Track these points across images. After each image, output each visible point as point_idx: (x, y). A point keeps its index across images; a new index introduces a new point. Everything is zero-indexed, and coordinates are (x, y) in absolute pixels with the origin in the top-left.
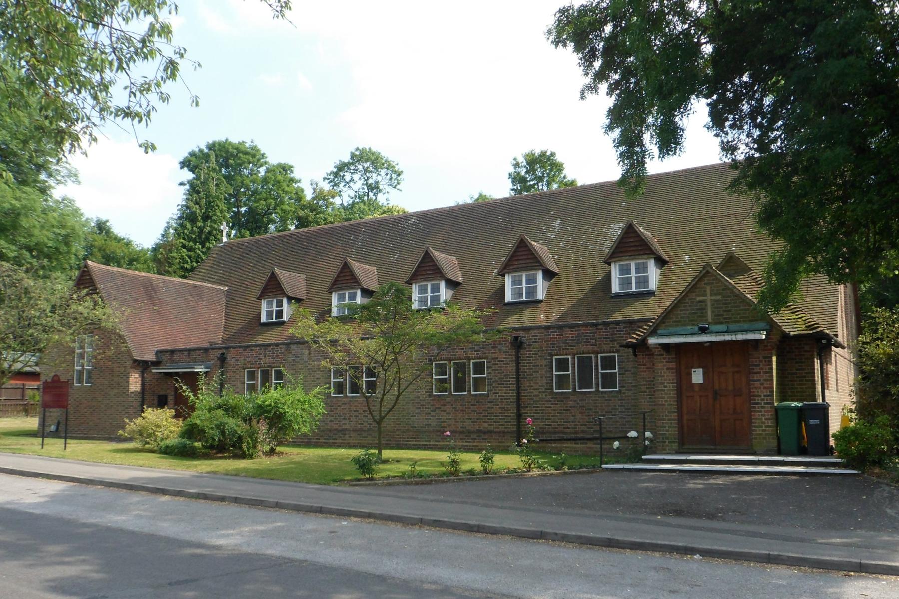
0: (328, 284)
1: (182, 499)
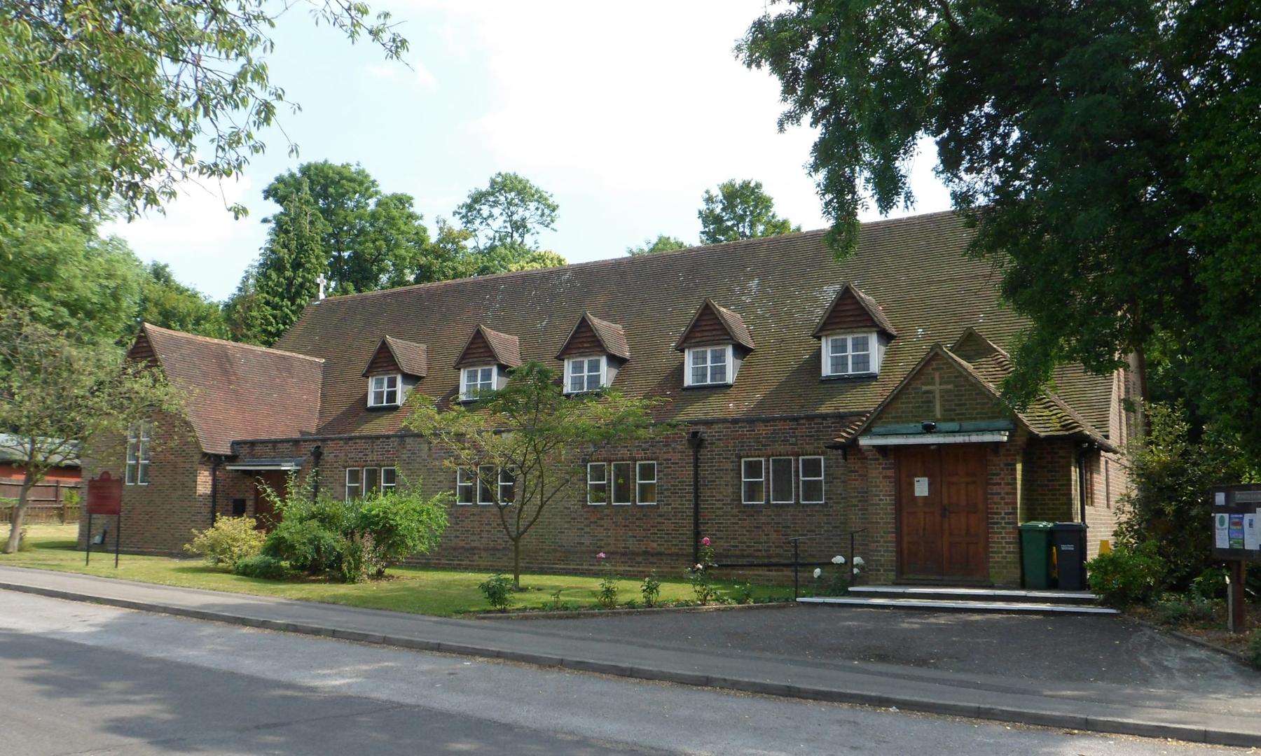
0: (454, 359)
1: (267, 631)
